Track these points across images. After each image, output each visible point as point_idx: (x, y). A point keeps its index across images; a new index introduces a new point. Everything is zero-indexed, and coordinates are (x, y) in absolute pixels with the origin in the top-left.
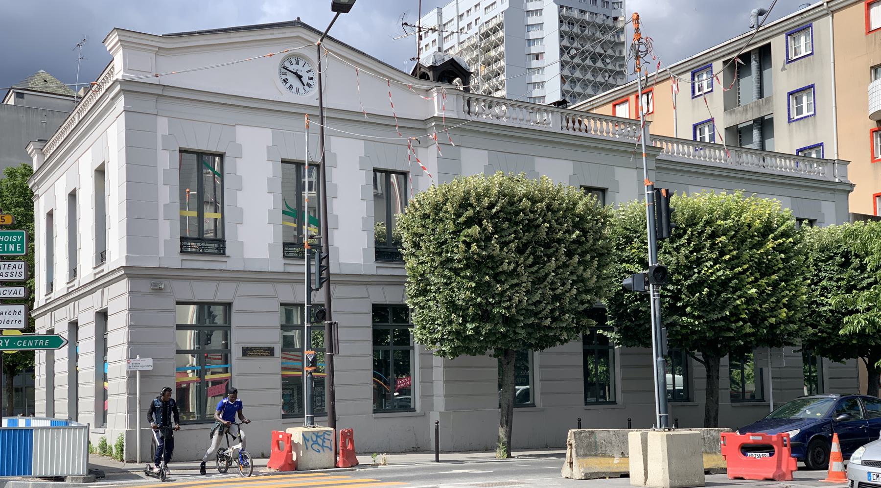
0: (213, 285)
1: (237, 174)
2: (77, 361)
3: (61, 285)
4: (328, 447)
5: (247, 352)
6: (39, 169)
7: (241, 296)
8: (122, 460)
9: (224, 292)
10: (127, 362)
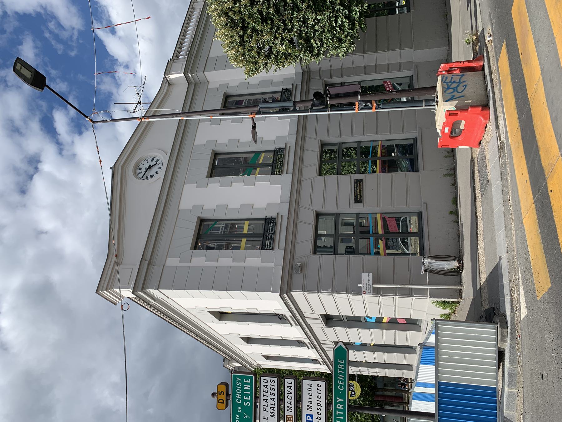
0: (300, 225)
1: (215, 208)
2: (370, 362)
3: (311, 353)
4: (460, 78)
5: (358, 199)
6: (239, 363)
7: (311, 204)
8: (458, 303)
9: (308, 218)
10: (364, 294)
